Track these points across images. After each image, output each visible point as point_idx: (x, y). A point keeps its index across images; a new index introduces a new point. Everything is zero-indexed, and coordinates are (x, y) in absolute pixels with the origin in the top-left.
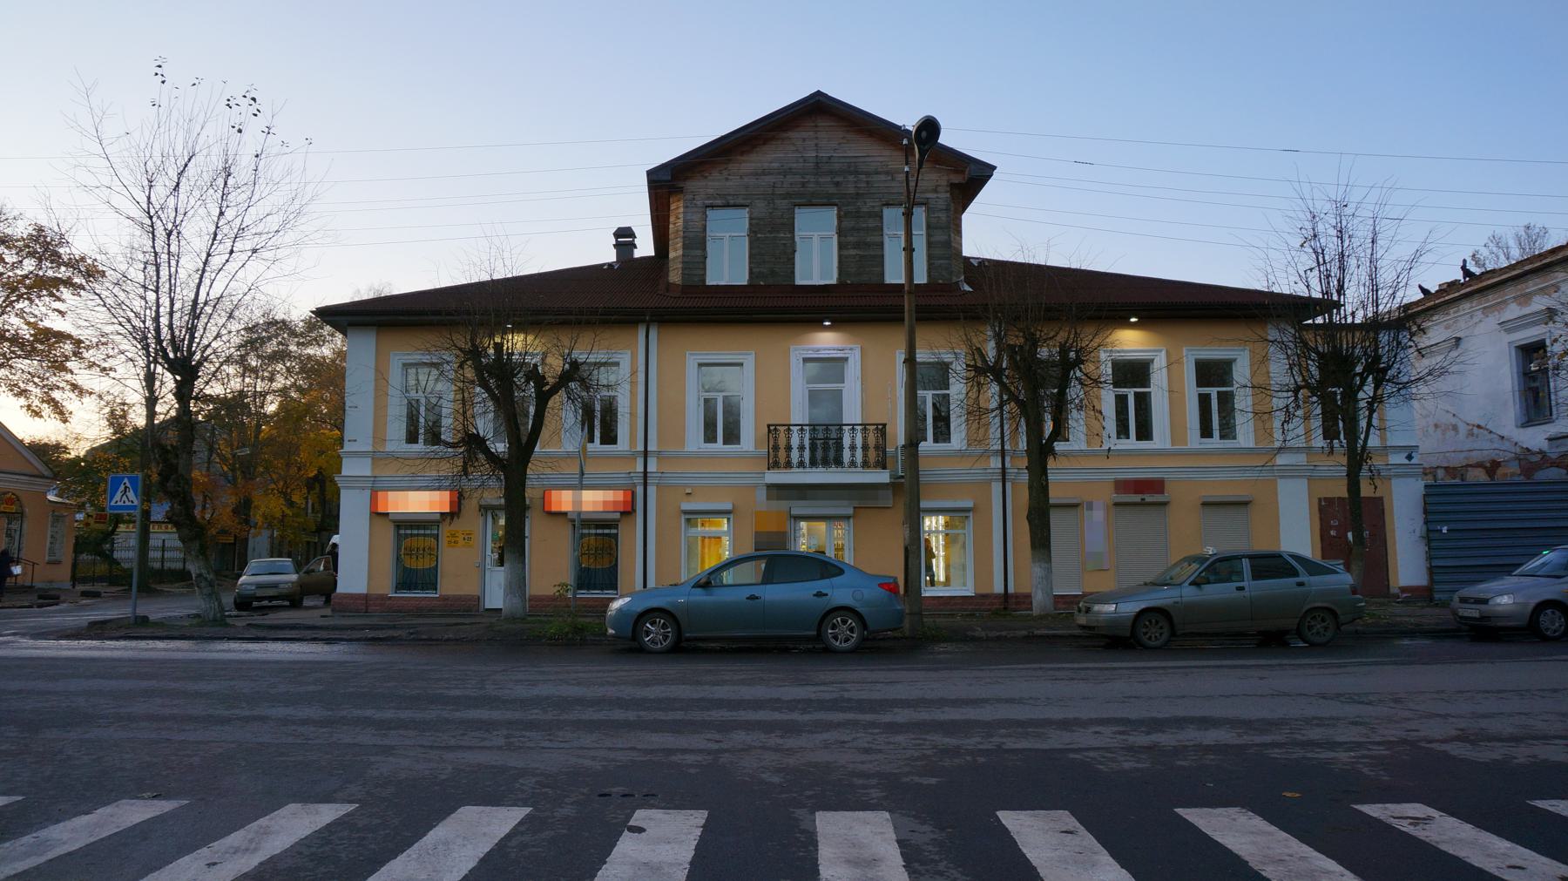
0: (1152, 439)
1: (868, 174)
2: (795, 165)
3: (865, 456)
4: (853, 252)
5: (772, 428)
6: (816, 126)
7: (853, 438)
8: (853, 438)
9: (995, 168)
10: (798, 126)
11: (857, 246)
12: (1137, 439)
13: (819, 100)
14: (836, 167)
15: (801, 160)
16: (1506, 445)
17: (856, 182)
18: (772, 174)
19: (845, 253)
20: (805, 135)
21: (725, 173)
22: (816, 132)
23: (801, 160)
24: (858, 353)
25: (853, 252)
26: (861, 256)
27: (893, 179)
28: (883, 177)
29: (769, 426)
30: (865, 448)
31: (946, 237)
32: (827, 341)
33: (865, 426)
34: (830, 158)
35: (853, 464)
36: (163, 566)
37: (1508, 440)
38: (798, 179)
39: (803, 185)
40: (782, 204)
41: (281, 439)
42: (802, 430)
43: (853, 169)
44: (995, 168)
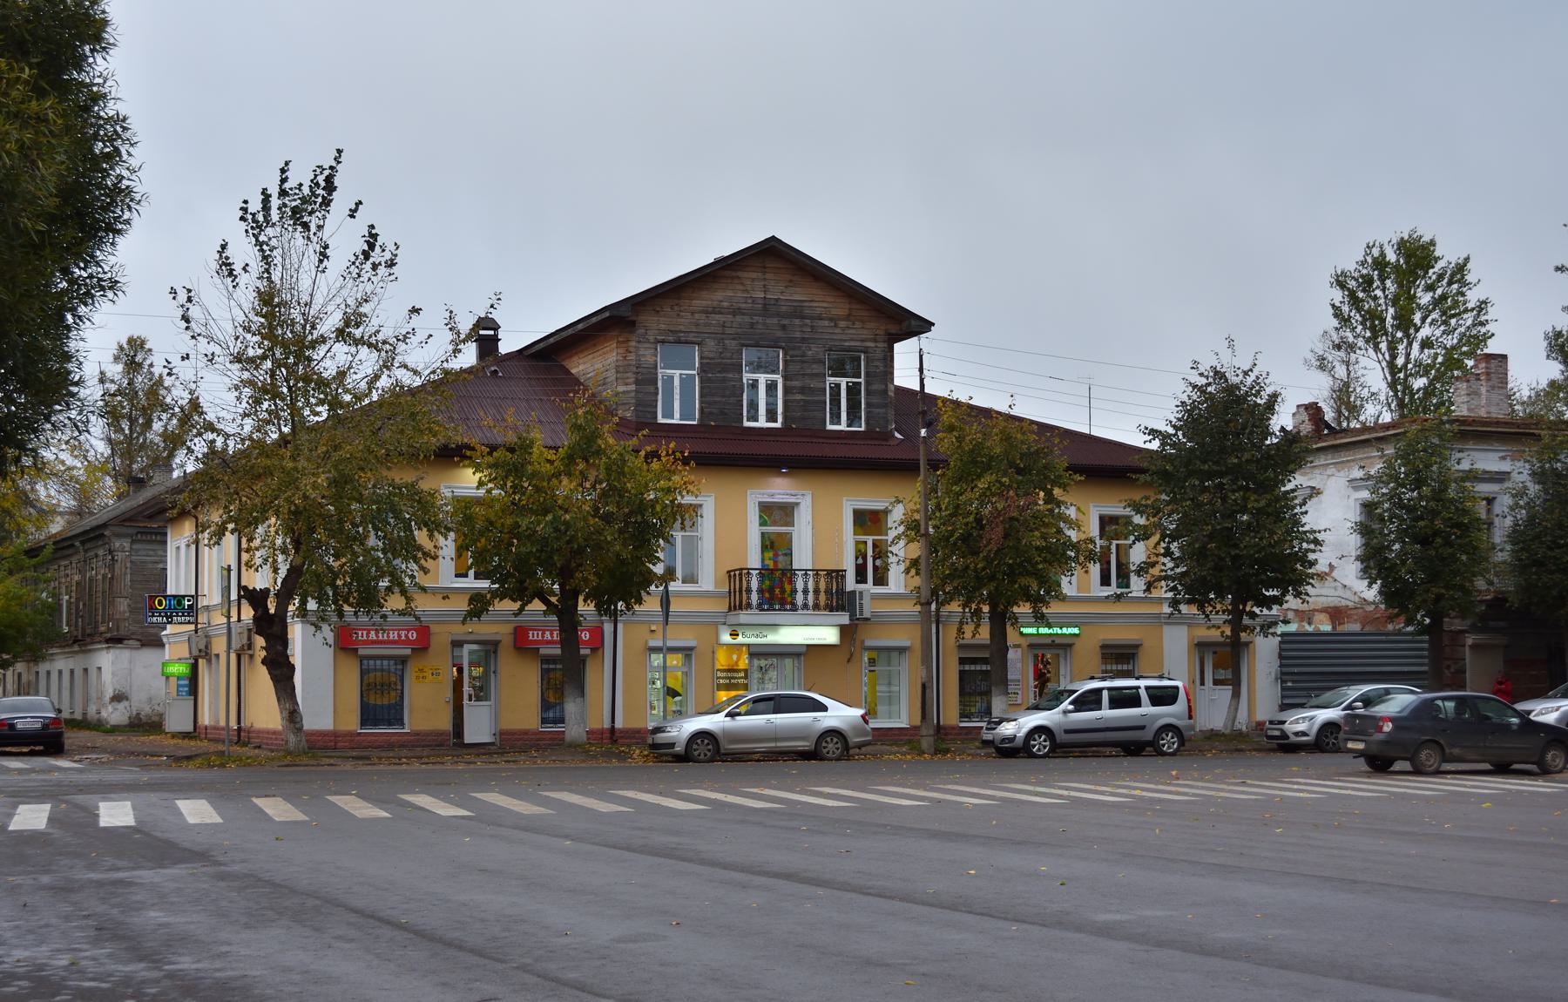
0: (1102, 585)
1: (812, 318)
2: (744, 305)
3: (817, 598)
4: (799, 397)
5: (732, 573)
6: (765, 268)
7: (806, 583)
8: (806, 583)
9: (933, 324)
10: (747, 266)
11: (803, 390)
12: (874, 585)
13: (773, 246)
14: (784, 309)
15: (750, 301)
16: (1348, 595)
17: (801, 326)
18: (722, 313)
19: (791, 397)
20: (754, 275)
21: (676, 308)
22: (764, 273)
23: (750, 301)
24: (809, 498)
25: (799, 397)
26: (804, 401)
27: (836, 326)
28: (826, 323)
29: (729, 572)
30: (817, 591)
31: (883, 387)
32: (779, 488)
33: (817, 572)
34: (777, 300)
35: (805, 606)
36: (665, 658)
37: (1350, 589)
38: (747, 319)
39: (752, 325)
40: (731, 344)
41: (592, 577)
42: (817, 574)
43: (798, 312)
44: (933, 324)
